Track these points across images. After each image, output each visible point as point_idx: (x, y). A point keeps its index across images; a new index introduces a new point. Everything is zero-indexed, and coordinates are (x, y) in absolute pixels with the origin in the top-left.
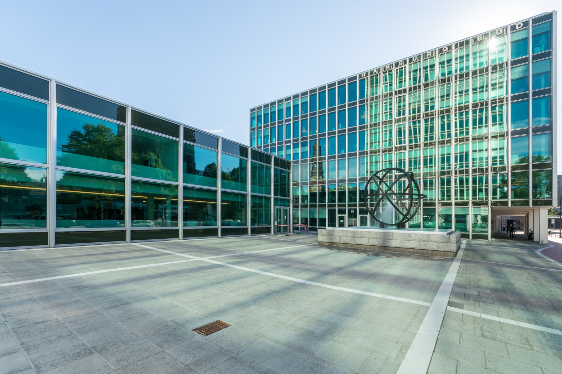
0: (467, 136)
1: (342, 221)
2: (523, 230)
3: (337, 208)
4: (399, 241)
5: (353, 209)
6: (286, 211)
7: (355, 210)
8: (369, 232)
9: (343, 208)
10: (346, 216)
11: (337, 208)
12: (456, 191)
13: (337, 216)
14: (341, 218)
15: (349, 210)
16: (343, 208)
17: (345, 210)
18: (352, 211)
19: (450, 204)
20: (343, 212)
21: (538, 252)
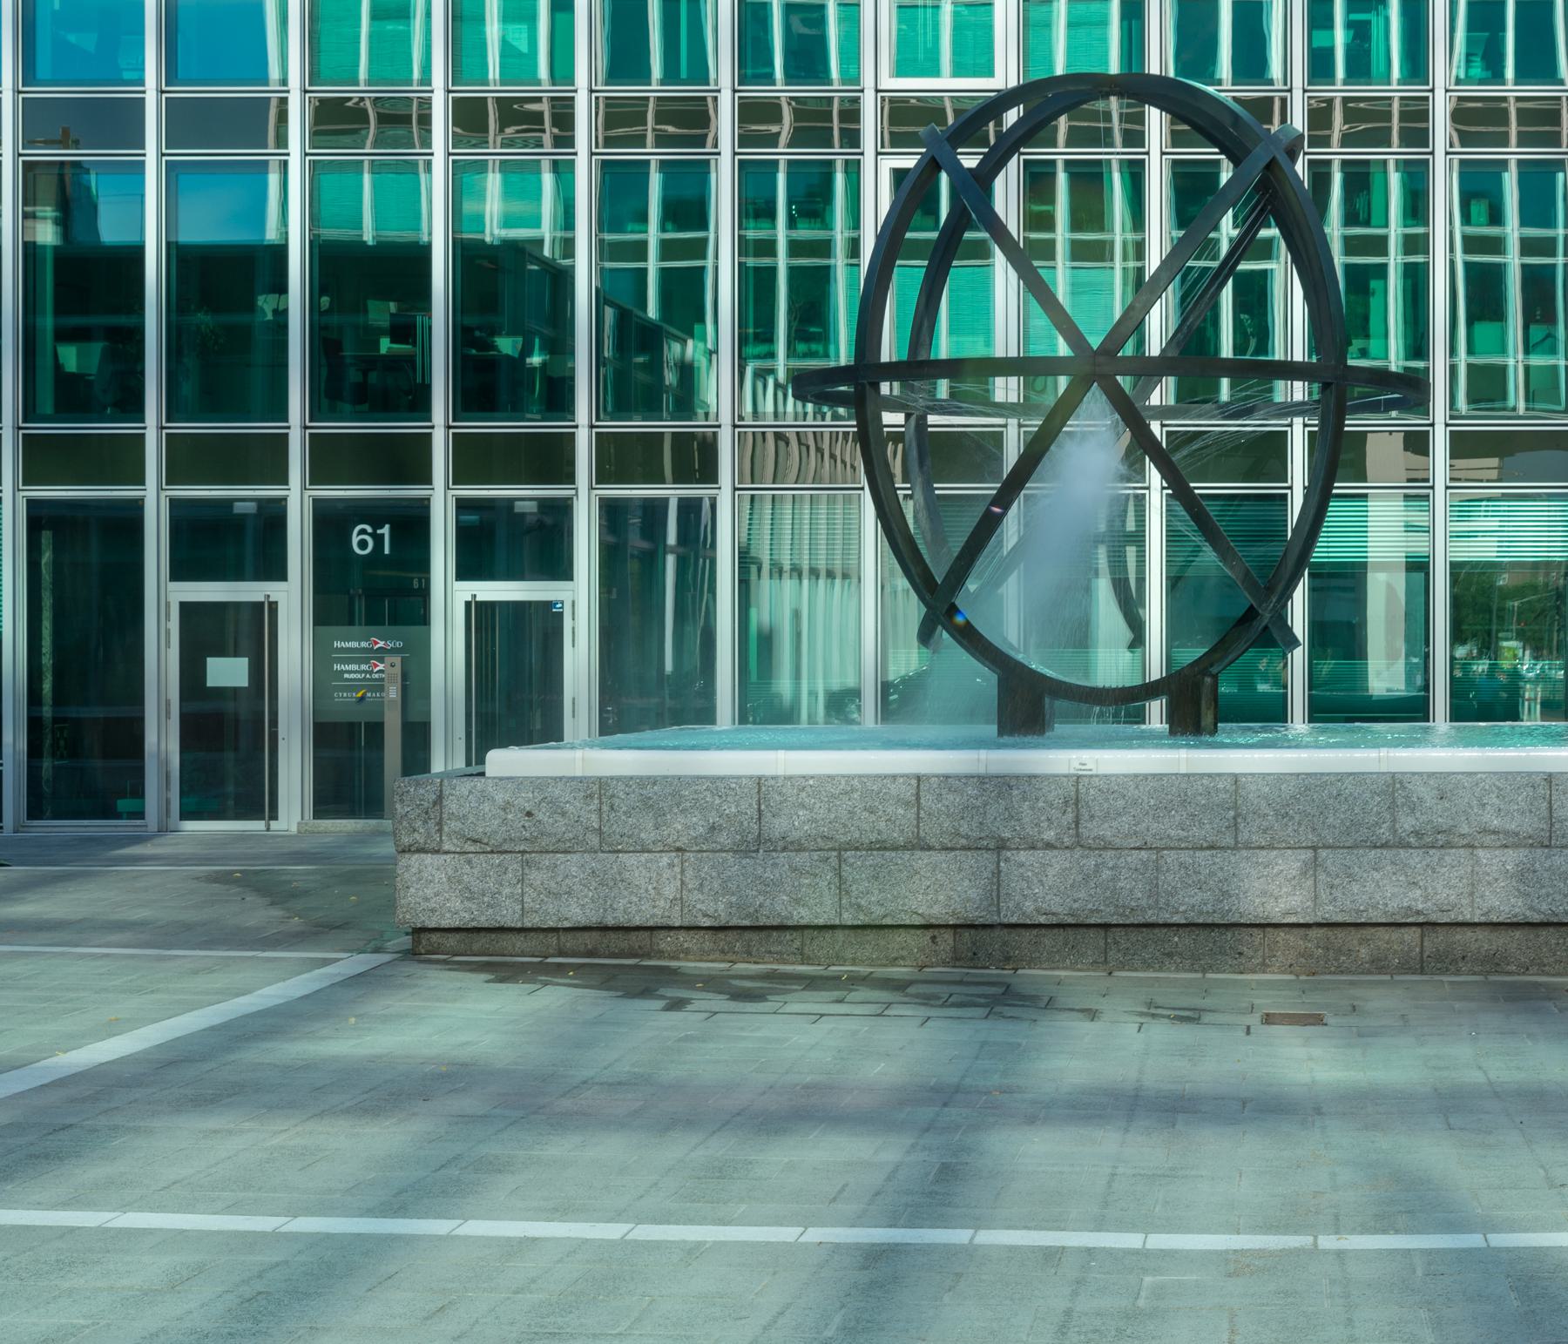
0: (1415, 90)
1: (227, 672)
2: (1239, 347)
3: (154, 497)
4: (1498, 862)
5: (372, 513)
6: (689, 509)
7: (411, 525)
8: (112, 1029)
9: (245, 494)
10: (290, 596)
11: (154, 497)
12: (1417, 206)
13: (165, 598)
14: (205, 631)
15: (331, 524)
16: (245, 494)
17: (273, 518)
18: (360, 539)
19: (402, 120)
20: (246, 543)
21: (1132, 264)
